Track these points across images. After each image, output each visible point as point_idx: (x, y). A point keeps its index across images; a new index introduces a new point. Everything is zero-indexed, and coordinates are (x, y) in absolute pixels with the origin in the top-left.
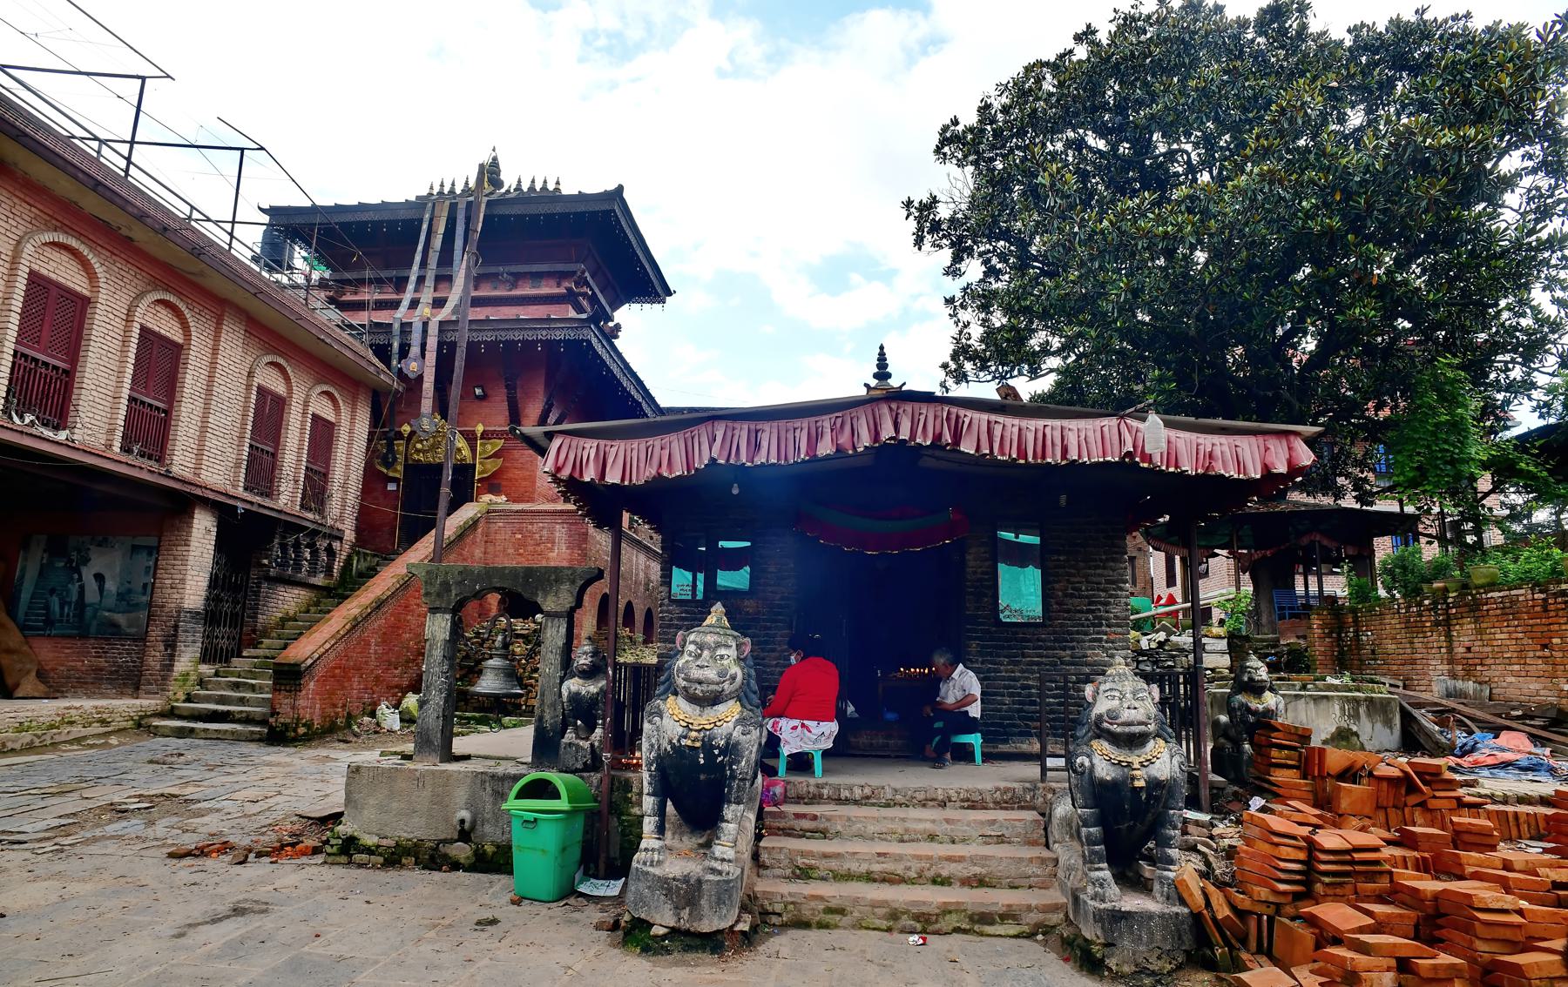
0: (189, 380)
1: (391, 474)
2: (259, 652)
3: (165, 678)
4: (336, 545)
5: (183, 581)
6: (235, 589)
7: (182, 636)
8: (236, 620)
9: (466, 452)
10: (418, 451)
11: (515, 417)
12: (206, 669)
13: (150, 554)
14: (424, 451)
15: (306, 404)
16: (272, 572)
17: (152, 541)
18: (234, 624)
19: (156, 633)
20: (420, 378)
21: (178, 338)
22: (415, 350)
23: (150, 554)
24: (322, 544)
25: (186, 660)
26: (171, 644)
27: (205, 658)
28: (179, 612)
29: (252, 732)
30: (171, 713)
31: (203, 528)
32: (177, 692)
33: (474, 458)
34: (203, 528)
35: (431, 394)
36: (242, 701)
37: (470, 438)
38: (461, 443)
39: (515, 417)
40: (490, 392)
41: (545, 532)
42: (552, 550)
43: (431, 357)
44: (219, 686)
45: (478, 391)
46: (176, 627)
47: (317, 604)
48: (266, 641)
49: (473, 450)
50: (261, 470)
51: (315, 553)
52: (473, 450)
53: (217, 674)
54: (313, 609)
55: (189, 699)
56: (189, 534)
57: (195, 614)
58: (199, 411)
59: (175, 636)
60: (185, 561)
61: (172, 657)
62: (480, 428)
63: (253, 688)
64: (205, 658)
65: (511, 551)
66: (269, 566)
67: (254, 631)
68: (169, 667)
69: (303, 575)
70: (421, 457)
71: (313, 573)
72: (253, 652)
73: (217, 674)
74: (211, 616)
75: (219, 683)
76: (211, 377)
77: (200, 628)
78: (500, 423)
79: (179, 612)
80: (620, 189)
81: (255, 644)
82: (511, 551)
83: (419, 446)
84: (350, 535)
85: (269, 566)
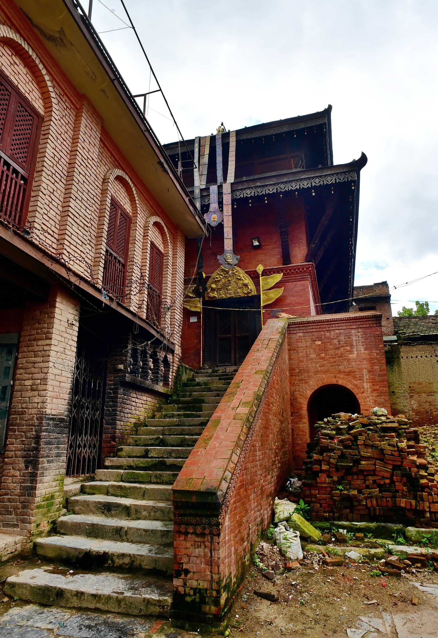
0: (49, 151)
1: (193, 309)
2: (124, 461)
3: (26, 505)
4: (170, 357)
5: (44, 380)
6: (94, 394)
7: (44, 449)
8: (96, 428)
9: (252, 286)
10: (213, 290)
11: (286, 258)
12: (72, 485)
13: (10, 353)
14: (218, 290)
15: (145, 236)
16: (128, 378)
17: (12, 338)
18: (93, 433)
19: (15, 446)
20: (221, 226)
21: (41, 111)
22: (214, 206)
23: (10, 353)
24: (161, 355)
25: (52, 480)
26: (32, 461)
27: (71, 471)
28: (40, 419)
29: (148, 602)
30: (31, 556)
31: (64, 318)
32: (40, 520)
33: (258, 290)
34: (64, 318)
35: (231, 236)
36: (118, 534)
37: (255, 277)
38: (248, 280)
39: (286, 258)
40: (263, 244)
41: (342, 338)
42: (351, 352)
43: (228, 209)
44: (87, 508)
45: (256, 243)
46: (38, 438)
47: (159, 409)
48: (126, 448)
49: (257, 284)
50: (116, 268)
51: (156, 362)
52: (257, 284)
53: (83, 491)
54: (158, 414)
55: (56, 529)
56: (51, 325)
57: (58, 421)
58: (59, 194)
59: (37, 449)
60: (46, 357)
61: (33, 478)
62: (260, 268)
63: (127, 512)
64: (71, 471)
65: (313, 356)
66: (124, 371)
67: (113, 438)
68: (30, 490)
69: (148, 382)
70: (215, 294)
71: (156, 381)
72: (116, 461)
73: (83, 491)
74: (74, 424)
75: (86, 504)
76: (71, 164)
77: (64, 438)
78: (274, 261)
79: (40, 419)
80: (328, 111)
81: (115, 452)
82: (313, 356)
83: (214, 286)
84: (178, 350)
85: (124, 371)
